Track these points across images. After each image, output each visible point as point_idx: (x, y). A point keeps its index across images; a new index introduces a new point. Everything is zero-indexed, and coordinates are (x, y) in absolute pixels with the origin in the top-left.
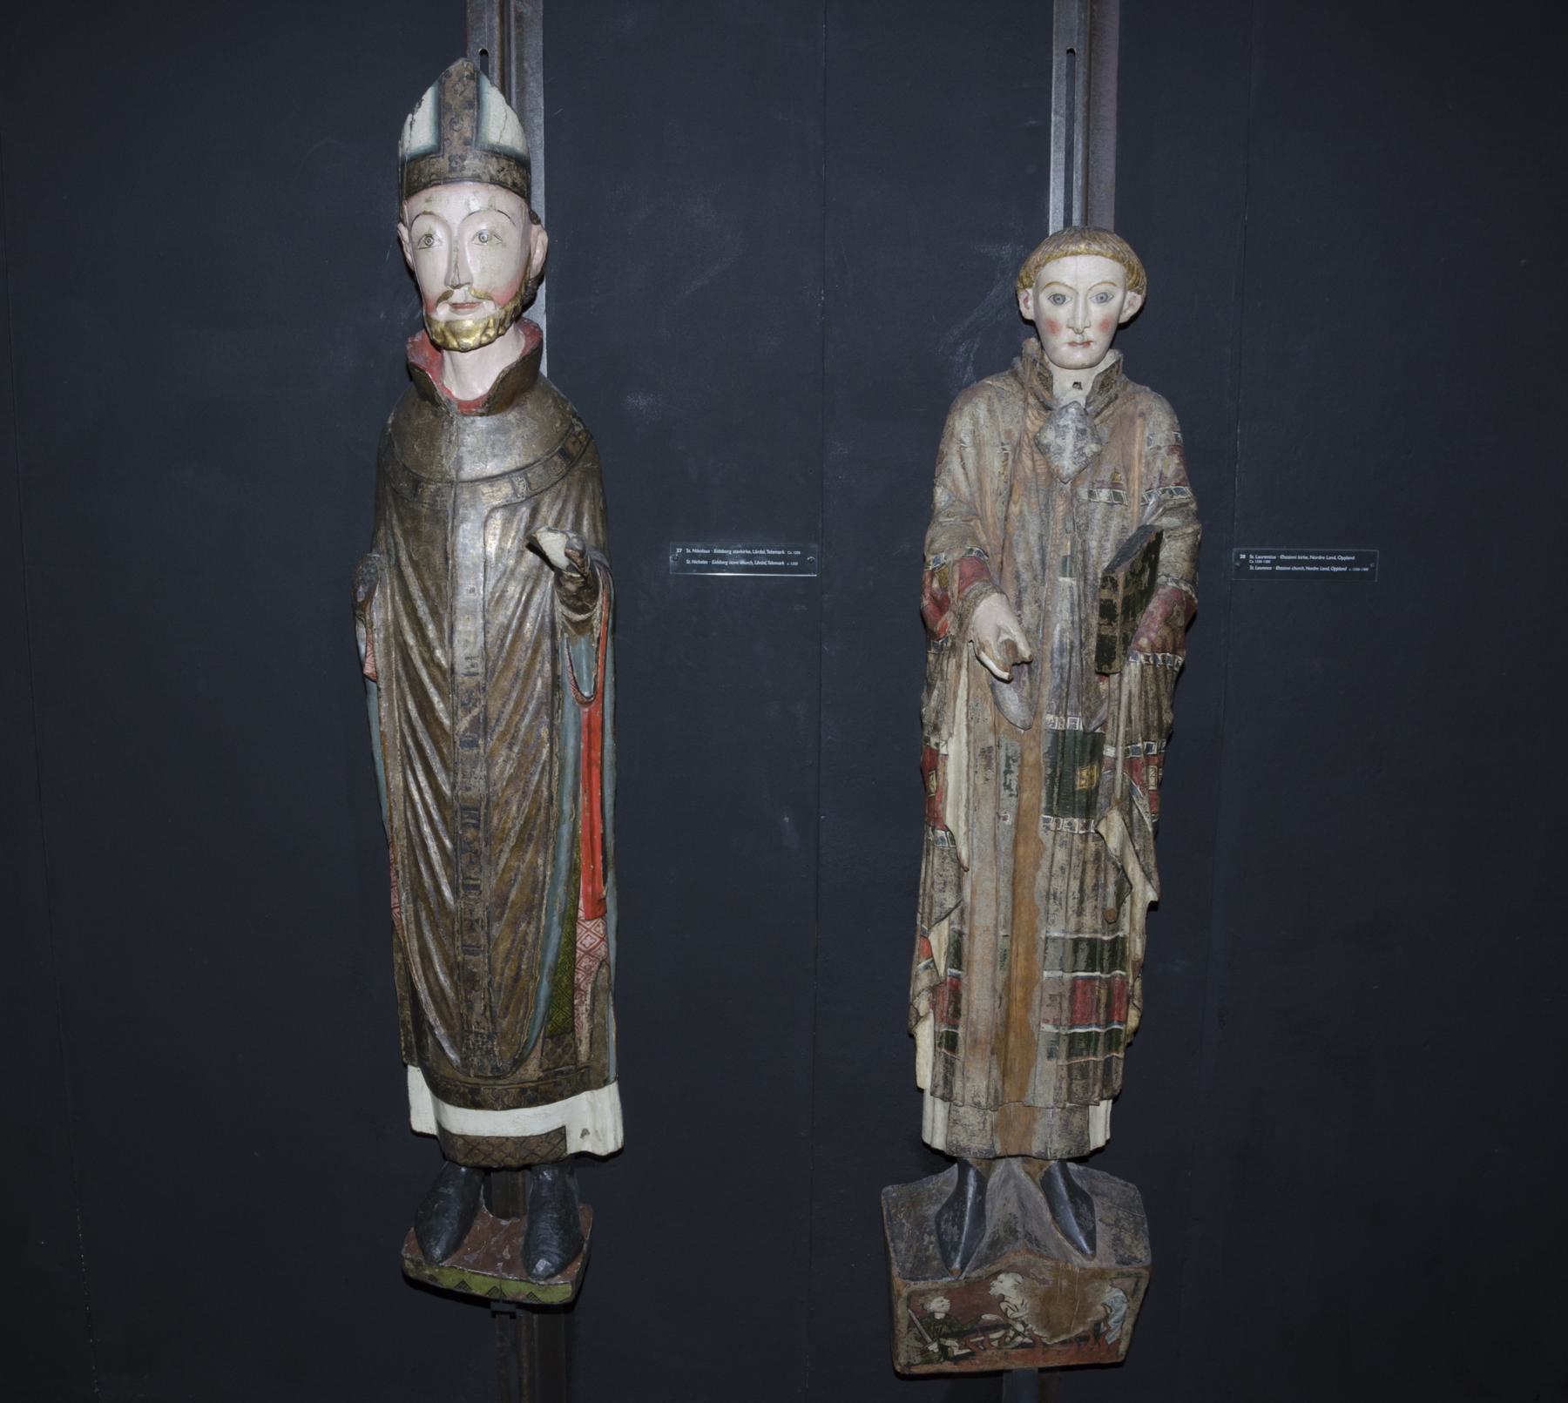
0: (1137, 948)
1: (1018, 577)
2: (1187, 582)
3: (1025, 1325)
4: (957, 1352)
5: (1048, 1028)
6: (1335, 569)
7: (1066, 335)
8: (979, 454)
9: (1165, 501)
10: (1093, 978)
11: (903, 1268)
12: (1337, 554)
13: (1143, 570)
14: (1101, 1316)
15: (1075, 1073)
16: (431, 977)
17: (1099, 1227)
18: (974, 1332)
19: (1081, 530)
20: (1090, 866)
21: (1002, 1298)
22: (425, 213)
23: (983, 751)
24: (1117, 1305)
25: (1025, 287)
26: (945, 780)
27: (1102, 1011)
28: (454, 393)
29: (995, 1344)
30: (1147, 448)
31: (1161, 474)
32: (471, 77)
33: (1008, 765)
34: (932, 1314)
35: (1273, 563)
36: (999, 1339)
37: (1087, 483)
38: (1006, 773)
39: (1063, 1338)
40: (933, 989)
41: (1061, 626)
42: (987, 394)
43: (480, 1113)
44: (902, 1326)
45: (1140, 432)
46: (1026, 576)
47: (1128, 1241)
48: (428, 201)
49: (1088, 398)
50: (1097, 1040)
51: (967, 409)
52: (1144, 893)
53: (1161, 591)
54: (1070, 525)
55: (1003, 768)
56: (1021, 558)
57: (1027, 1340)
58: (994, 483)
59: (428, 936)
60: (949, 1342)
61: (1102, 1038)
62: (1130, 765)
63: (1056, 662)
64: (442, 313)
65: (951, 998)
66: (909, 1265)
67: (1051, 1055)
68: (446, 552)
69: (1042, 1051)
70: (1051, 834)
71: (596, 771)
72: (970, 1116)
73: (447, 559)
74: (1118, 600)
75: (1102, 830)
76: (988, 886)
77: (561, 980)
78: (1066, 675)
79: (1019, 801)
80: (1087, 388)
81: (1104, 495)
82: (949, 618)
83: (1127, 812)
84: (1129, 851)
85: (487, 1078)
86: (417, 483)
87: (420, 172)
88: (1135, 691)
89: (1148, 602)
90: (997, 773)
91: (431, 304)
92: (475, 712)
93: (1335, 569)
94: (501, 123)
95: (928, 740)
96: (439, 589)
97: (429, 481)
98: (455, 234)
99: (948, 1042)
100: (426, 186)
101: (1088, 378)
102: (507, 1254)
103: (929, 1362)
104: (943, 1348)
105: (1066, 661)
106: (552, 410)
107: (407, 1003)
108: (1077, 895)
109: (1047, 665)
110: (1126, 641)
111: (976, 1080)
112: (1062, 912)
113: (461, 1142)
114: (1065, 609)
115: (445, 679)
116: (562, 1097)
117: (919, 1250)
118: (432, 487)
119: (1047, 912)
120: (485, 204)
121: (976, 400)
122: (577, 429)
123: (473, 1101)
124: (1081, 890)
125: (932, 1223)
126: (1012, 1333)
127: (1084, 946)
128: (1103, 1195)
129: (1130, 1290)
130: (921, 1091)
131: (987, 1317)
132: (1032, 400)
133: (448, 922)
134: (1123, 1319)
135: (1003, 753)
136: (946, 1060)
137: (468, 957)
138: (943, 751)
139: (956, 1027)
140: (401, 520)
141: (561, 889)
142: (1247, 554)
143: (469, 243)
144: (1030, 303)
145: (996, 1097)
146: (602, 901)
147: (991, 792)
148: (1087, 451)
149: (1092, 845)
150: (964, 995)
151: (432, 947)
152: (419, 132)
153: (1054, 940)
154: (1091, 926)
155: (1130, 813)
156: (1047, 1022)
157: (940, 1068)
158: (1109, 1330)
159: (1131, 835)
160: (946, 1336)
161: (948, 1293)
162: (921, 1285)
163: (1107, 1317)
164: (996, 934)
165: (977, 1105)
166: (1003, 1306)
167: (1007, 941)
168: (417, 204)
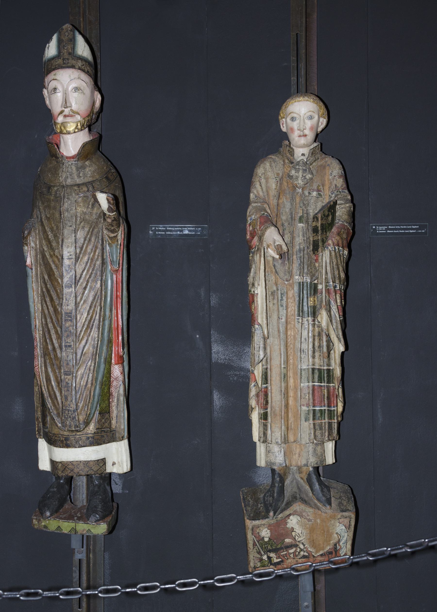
0: (338, 372)
1: (283, 225)
2: (347, 222)
3: (304, 545)
4: (276, 560)
5: (304, 408)
6: (411, 231)
7: (297, 133)
8: (267, 182)
9: (338, 195)
10: (321, 386)
11: (249, 516)
12: (411, 225)
13: (328, 215)
14: (336, 540)
15: (317, 427)
16: (50, 388)
17: (333, 499)
18: (281, 548)
19: (306, 205)
20: (316, 338)
21: (293, 530)
22: (54, 80)
23: (272, 293)
24: (343, 534)
25: (282, 118)
26: (257, 304)
27: (326, 400)
28: (65, 154)
29: (292, 556)
30: (331, 177)
31: (336, 185)
32: (71, 30)
33: (282, 297)
34: (263, 538)
35: (386, 230)
36: (293, 553)
37: (308, 189)
38: (281, 300)
39: (321, 552)
40: (257, 395)
41: (299, 240)
42: (269, 160)
43: (69, 449)
44: (250, 545)
45: (328, 171)
46: (286, 224)
47: (345, 503)
48: (55, 75)
49: (307, 159)
50: (325, 412)
51: (262, 165)
52: (339, 348)
53: (336, 225)
54: (302, 205)
55: (280, 298)
56: (284, 218)
57: (306, 554)
58: (273, 192)
59: (49, 370)
60: (272, 555)
61: (326, 411)
62: (328, 291)
63: (298, 256)
64: (60, 119)
65: (264, 395)
66: (252, 515)
67: (307, 420)
68: (61, 212)
69: (303, 419)
70: (300, 324)
71: (119, 300)
72: (276, 449)
73: (61, 215)
74: (319, 225)
75: (319, 320)
76: (277, 347)
77: (104, 389)
78: (302, 260)
79: (287, 312)
80: (307, 156)
81: (315, 194)
82: (256, 239)
83: (329, 311)
84: (331, 328)
85: (72, 431)
86: (49, 188)
87: (52, 65)
88: (328, 261)
89: (331, 229)
90: (278, 301)
91: (55, 117)
92: (71, 274)
93: (411, 231)
94: (82, 49)
95: (250, 291)
96: (57, 227)
97: (54, 186)
98: (65, 87)
99: (264, 417)
100: (54, 70)
101: (306, 151)
102: (79, 515)
103: (263, 566)
104: (269, 558)
105: (302, 254)
106: (103, 163)
107: (39, 409)
108: (312, 349)
109: (295, 257)
110: (323, 242)
111: (276, 433)
112: (307, 357)
113: (60, 465)
114: (301, 234)
115: (59, 261)
116: (105, 443)
117: (256, 509)
118: (56, 188)
119: (301, 358)
120: (77, 77)
121: (265, 162)
122: (112, 171)
123: (66, 444)
124: (314, 347)
125: (262, 499)
126: (298, 550)
127: (316, 371)
128: (334, 488)
129: (347, 525)
130: (255, 443)
131: (287, 540)
132: (287, 161)
133: (58, 363)
134: (346, 542)
135: (279, 292)
136: (264, 424)
137: (66, 377)
138: (256, 292)
139: (267, 409)
140: (43, 203)
141: (105, 348)
142: (376, 226)
143: (69, 94)
144: (284, 125)
145: (285, 438)
146: (122, 357)
147: (276, 309)
148: (307, 177)
149: (317, 329)
150: (270, 394)
151: (51, 375)
152: (51, 50)
153: (304, 369)
154: (319, 363)
155: (330, 311)
156: (304, 405)
157: (262, 429)
158: (341, 548)
159: (331, 321)
160: (270, 551)
161: (270, 527)
162: (257, 522)
163: (339, 541)
164: (281, 367)
165: (277, 443)
166: (293, 534)
167: (285, 370)
168: (51, 76)
